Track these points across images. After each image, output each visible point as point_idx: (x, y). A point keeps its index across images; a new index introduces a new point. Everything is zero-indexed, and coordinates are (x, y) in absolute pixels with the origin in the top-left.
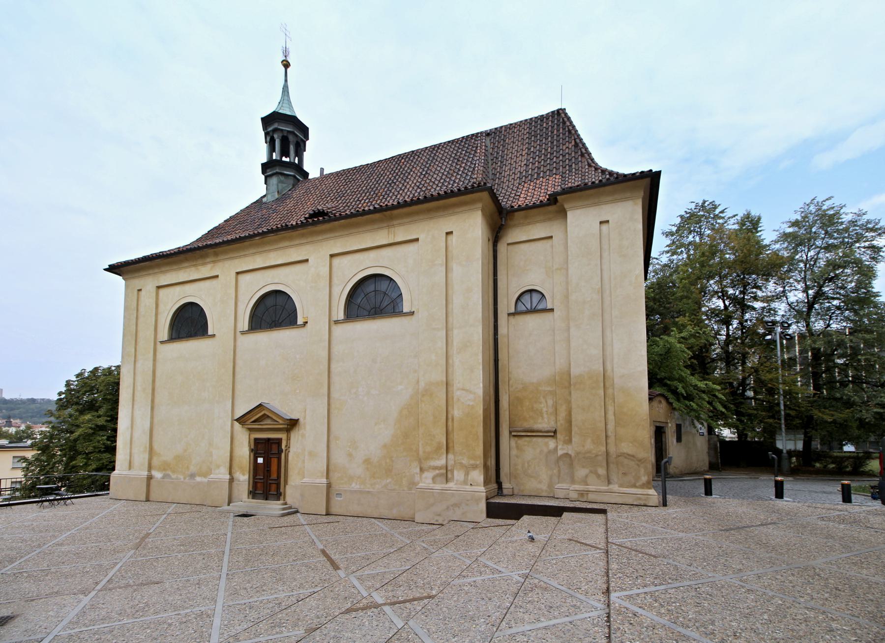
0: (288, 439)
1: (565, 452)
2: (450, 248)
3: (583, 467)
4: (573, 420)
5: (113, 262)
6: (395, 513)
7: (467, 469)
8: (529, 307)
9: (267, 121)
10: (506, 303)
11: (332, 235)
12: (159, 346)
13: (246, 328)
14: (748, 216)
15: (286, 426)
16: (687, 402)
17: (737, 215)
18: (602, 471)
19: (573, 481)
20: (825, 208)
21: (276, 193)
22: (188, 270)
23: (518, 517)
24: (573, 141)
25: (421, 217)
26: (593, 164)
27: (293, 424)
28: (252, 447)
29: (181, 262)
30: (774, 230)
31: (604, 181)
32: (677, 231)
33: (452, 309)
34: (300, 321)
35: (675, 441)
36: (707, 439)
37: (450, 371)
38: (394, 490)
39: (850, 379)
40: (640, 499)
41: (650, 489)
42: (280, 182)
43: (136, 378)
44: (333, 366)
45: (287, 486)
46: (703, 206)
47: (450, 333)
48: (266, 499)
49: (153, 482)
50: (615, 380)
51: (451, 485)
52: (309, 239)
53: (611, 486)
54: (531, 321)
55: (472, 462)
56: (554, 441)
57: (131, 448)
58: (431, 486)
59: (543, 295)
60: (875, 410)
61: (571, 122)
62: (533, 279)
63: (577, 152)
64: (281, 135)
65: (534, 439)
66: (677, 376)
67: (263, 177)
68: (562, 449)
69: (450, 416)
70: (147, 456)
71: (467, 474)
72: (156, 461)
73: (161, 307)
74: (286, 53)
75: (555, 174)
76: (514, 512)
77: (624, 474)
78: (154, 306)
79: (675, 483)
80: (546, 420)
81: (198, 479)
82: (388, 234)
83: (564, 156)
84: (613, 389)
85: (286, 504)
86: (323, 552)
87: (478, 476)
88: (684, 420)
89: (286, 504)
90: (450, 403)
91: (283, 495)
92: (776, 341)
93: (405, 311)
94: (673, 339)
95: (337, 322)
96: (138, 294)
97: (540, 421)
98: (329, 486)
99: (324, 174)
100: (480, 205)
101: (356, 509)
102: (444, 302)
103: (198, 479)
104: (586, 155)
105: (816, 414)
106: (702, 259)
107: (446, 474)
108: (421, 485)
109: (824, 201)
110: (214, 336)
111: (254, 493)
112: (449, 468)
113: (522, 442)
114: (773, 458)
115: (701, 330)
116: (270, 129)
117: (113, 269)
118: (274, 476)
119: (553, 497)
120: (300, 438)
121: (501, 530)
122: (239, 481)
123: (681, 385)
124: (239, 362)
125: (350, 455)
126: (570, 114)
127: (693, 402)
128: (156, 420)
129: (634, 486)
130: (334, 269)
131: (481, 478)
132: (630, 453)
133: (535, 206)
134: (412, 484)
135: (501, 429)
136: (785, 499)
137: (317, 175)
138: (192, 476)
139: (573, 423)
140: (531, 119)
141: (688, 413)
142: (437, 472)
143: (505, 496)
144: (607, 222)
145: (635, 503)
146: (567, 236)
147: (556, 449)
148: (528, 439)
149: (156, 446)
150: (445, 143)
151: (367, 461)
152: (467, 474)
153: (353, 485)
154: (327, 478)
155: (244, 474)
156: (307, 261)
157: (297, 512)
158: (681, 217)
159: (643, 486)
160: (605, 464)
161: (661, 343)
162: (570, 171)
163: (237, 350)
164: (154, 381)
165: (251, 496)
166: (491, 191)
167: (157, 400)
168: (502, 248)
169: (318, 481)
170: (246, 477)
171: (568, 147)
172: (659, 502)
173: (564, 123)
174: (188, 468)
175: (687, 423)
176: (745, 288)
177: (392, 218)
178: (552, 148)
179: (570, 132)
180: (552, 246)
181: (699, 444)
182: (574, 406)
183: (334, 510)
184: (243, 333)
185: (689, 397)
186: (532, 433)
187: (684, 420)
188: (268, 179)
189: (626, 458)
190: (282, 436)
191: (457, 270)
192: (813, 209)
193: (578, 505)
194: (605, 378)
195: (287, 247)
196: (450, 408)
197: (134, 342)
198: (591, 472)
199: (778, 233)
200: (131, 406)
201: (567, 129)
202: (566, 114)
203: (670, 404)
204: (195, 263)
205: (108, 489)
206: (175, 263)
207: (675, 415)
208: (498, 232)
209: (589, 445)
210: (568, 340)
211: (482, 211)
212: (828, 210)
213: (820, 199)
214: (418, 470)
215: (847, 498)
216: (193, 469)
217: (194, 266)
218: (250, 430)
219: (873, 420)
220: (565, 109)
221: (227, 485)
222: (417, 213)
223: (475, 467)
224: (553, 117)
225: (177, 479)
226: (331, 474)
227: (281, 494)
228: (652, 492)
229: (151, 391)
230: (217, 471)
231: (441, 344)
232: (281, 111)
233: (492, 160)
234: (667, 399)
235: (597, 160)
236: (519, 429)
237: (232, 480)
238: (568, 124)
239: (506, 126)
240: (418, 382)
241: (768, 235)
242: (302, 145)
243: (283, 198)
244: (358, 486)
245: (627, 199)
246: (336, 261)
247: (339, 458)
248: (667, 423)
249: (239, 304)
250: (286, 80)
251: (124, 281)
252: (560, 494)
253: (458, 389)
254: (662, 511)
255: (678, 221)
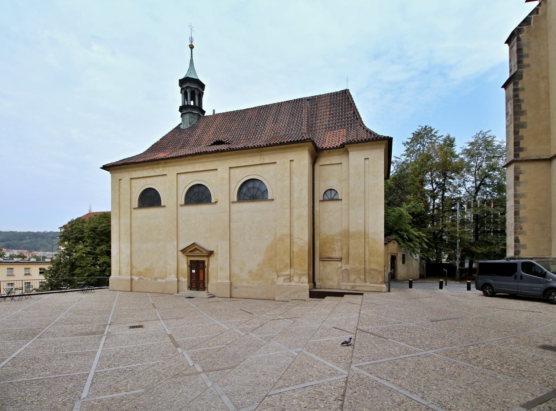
0: (209, 261)
1: (346, 268)
2: (292, 168)
3: (354, 275)
4: (350, 253)
5: (105, 164)
6: (265, 296)
7: (300, 276)
8: (330, 198)
9: (182, 82)
10: (318, 195)
11: (231, 157)
12: (133, 210)
13: (183, 203)
14: (448, 137)
15: (208, 254)
16: (408, 243)
17: (443, 136)
18: (362, 277)
19: (349, 281)
20: (487, 136)
21: (189, 124)
22: (149, 170)
23: (323, 297)
24: (353, 110)
25: (278, 152)
26: (362, 125)
27: (211, 253)
28: (189, 264)
29: (145, 166)
30: (460, 148)
31: (367, 139)
32: (411, 142)
33: (293, 199)
34: (213, 201)
35: (401, 263)
36: (419, 262)
37: (292, 229)
38: (264, 286)
39: (447, 242)
40: (378, 289)
41: (383, 284)
42: (191, 117)
43: (121, 227)
44: (231, 224)
45: (209, 284)
46: (425, 129)
47: (292, 210)
48: (198, 290)
49: (133, 281)
50: (370, 235)
51: (292, 283)
52: (218, 159)
53: (366, 284)
54: (331, 205)
55: (302, 272)
56: (341, 263)
57: (120, 264)
58: (283, 284)
59: (337, 192)
60: (501, 247)
61: (352, 99)
62: (333, 184)
63: (355, 117)
64: (191, 90)
65: (331, 262)
66: (404, 229)
67: (180, 114)
68: (344, 267)
69: (292, 251)
70: (129, 268)
71: (300, 278)
72: (134, 271)
73: (133, 190)
74: (191, 40)
75: (344, 128)
76: (321, 295)
77: (372, 278)
78: (129, 189)
79: (399, 284)
80: (337, 253)
81: (159, 280)
82: (261, 159)
83: (348, 118)
84: (369, 239)
85: (208, 293)
86: (170, 336)
87: (305, 279)
88: (406, 252)
89: (208, 293)
90: (292, 244)
91: (206, 288)
92: (457, 210)
93: (269, 198)
94: (404, 209)
95: (233, 202)
96: (119, 181)
97: (334, 253)
98: (231, 284)
99: (215, 113)
100: (307, 148)
101: (245, 295)
102: (289, 195)
103: (159, 280)
104: (359, 119)
105: (474, 249)
106: (422, 163)
107: (290, 278)
108: (278, 283)
109: (487, 132)
110: (165, 206)
111: (191, 288)
112: (291, 275)
113: (325, 263)
114: (445, 271)
115: (418, 204)
116: (184, 86)
117: (105, 168)
118: (201, 279)
119: (340, 289)
120: (215, 260)
121: (318, 302)
122: (182, 281)
123: (406, 234)
124: (180, 221)
125: (241, 269)
126: (351, 93)
127: (412, 243)
128: (133, 250)
129: (376, 283)
130: (231, 175)
131: (307, 280)
132: (375, 268)
133: (333, 148)
134: (273, 283)
135: (315, 257)
136: (443, 289)
137: (211, 114)
138: (156, 279)
139: (350, 255)
140: (331, 93)
141: (408, 249)
142: (286, 277)
143: (317, 288)
144: (368, 159)
145: (376, 291)
146: (349, 164)
147: (341, 267)
148: (328, 262)
149: (134, 264)
150: (284, 102)
151: (250, 272)
152: (300, 278)
153: (243, 283)
154: (230, 280)
155: (184, 278)
156: (217, 169)
157: (214, 296)
158: (413, 134)
159: (380, 283)
160: (364, 273)
161: (397, 211)
162: (351, 127)
163: (178, 215)
164: (131, 229)
165: (189, 289)
166: (313, 142)
167: (133, 239)
168: (317, 167)
169: (225, 281)
170: (186, 279)
171: (350, 113)
172: (387, 290)
173: (348, 98)
174: (153, 274)
175: (409, 254)
176: (445, 179)
177: (262, 151)
178: (342, 113)
179: (351, 104)
180: (342, 168)
181: (414, 265)
182: (350, 247)
183: (233, 295)
184: (181, 205)
185: (410, 240)
186: (330, 259)
187: (406, 252)
188: (184, 115)
189: (373, 270)
190: (206, 259)
191: (296, 180)
192: (481, 136)
193: (351, 292)
194: (366, 234)
195: (205, 162)
196: (292, 247)
197: (118, 208)
198: (357, 277)
199: (462, 149)
200: (118, 242)
201: (350, 103)
202: (349, 93)
203: (399, 244)
204: (153, 167)
205: (108, 285)
206: (142, 166)
207: (402, 249)
208: (315, 160)
209: (357, 265)
210: (349, 214)
211: (308, 150)
212: (488, 138)
213: (484, 131)
214: (276, 276)
215: (469, 288)
216: (156, 275)
217: (153, 168)
218: (187, 256)
219: (500, 252)
220: (349, 90)
221: (176, 283)
222: (276, 149)
223: (304, 275)
224: (342, 94)
225: (147, 280)
226: (232, 278)
227: (205, 288)
228: (384, 286)
229: (130, 234)
230: (170, 276)
231: (288, 216)
232: (190, 76)
233: (311, 115)
234: (398, 241)
235: (366, 125)
236: (325, 257)
237: (178, 281)
238: (350, 99)
239: (318, 96)
240: (276, 234)
241: (457, 150)
242: (202, 95)
243: (193, 128)
244: (246, 284)
245: (377, 148)
246: (232, 171)
247: (236, 270)
248: (398, 254)
249: (179, 190)
250: (192, 57)
251: (110, 174)
252: (343, 287)
253: (296, 238)
254: (388, 293)
255: (412, 136)
